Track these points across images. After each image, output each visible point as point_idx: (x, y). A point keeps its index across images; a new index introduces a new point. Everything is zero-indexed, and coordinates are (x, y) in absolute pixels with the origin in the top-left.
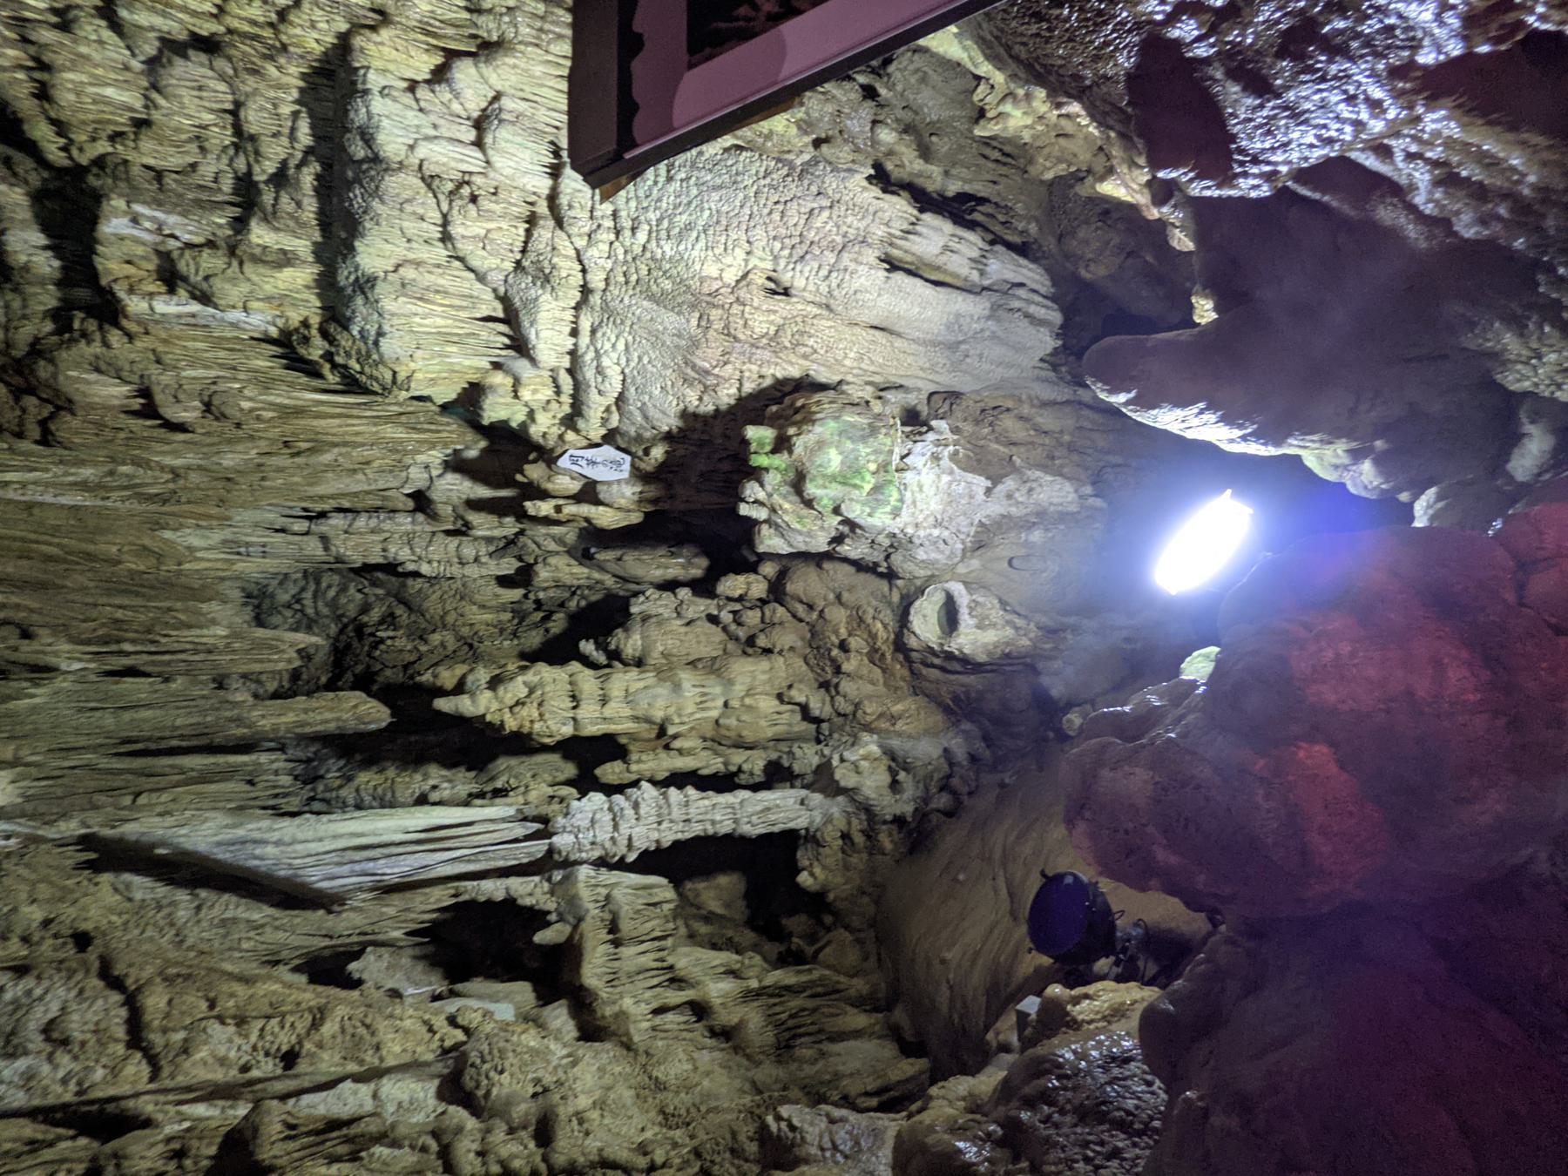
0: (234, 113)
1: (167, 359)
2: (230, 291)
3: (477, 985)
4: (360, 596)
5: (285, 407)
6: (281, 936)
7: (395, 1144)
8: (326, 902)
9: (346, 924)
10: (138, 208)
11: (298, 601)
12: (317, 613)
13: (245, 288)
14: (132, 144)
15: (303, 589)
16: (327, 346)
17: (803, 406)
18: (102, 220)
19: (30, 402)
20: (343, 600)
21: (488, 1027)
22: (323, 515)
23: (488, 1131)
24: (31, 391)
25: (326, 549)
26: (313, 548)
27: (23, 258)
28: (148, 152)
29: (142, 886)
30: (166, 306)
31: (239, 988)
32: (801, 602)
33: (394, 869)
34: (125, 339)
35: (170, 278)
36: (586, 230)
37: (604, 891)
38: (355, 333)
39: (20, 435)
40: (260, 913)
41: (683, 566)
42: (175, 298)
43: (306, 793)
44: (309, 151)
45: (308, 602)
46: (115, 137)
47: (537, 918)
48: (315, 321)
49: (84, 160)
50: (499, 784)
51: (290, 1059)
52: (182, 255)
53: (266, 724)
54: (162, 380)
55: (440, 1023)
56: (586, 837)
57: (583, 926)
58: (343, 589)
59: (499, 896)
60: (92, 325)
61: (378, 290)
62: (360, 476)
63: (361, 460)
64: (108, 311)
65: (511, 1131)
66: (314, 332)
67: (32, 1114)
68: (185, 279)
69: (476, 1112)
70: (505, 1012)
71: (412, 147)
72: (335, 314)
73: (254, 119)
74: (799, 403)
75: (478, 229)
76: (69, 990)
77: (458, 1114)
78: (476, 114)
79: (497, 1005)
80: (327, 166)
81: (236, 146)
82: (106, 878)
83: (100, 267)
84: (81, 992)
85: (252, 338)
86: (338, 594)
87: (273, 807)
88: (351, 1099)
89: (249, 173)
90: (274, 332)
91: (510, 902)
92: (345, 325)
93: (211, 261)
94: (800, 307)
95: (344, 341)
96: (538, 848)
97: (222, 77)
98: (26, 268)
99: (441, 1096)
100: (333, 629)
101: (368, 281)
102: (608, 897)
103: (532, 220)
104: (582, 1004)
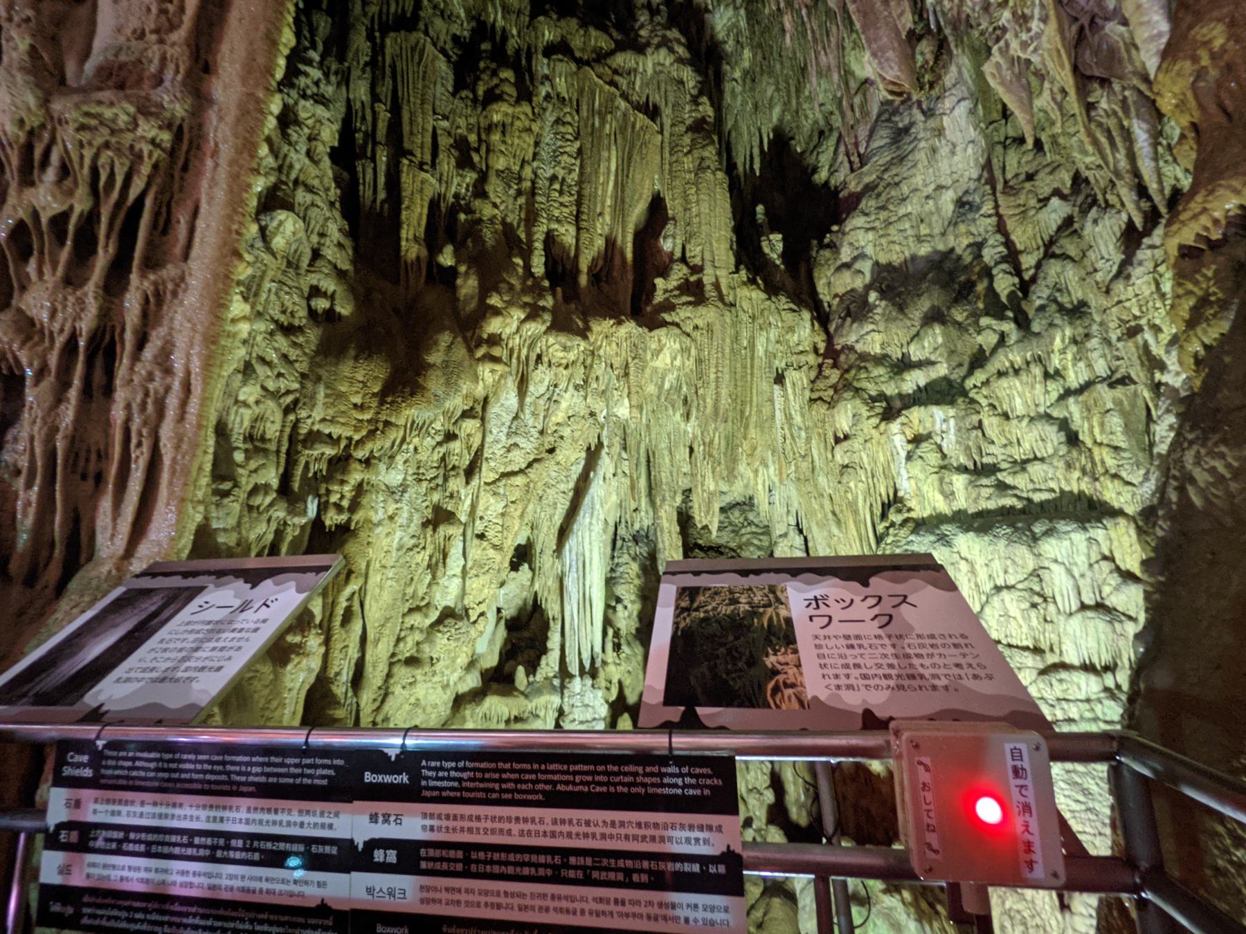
0: (1036, 458)
2: (916, 468)
3: (502, 632)
6: (545, 529)
7: (430, 585)
8: (559, 550)
9: (546, 560)
10: (952, 422)
13: (921, 476)
17: (937, 913)
19: (831, 392)
21: (473, 633)
22: (801, 531)
23: (421, 631)
24: (836, 391)
26: (779, 529)
28: (991, 424)
29: (577, 469)
31: (519, 513)
32: (765, 914)
33: (570, 583)
36: (1045, 695)
37: (542, 714)
40: (558, 519)
41: (797, 800)
43: (628, 537)
44: (1029, 500)
46: (993, 407)
47: (532, 668)
48: (913, 515)
49: (972, 394)
50: (624, 647)
51: (481, 536)
53: (662, 513)
54: (856, 444)
55: (483, 608)
56: (576, 701)
57: (522, 698)
58: (759, 548)
59: (549, 645)
64: (889, 415)
65: (418, 643)
67: (482, 445)
69: (432, 626)
70: (482, 647)
71: (1056, 561)
73: (1035, 469)
74: (939, 908)
75: (1014, 610)
77: (434, 615)
78: (1107, 603)
79: (486, 642)
80: (1023, 511)
81: (1015, 462)
82: (583, 455)
88: (455, 563)
89: (1000, 470)
90: (900, 494)
91: (544, 650)
92: (915, 531)
93: (934, 459)
94: (1053, 923)
95: (903, 532)
96: (574, 668)
97: (1056, 451)
99: (447, 608)
100: (733, 545)
102: (537, 716)
103: (1037, 651)
104: (476, 696)
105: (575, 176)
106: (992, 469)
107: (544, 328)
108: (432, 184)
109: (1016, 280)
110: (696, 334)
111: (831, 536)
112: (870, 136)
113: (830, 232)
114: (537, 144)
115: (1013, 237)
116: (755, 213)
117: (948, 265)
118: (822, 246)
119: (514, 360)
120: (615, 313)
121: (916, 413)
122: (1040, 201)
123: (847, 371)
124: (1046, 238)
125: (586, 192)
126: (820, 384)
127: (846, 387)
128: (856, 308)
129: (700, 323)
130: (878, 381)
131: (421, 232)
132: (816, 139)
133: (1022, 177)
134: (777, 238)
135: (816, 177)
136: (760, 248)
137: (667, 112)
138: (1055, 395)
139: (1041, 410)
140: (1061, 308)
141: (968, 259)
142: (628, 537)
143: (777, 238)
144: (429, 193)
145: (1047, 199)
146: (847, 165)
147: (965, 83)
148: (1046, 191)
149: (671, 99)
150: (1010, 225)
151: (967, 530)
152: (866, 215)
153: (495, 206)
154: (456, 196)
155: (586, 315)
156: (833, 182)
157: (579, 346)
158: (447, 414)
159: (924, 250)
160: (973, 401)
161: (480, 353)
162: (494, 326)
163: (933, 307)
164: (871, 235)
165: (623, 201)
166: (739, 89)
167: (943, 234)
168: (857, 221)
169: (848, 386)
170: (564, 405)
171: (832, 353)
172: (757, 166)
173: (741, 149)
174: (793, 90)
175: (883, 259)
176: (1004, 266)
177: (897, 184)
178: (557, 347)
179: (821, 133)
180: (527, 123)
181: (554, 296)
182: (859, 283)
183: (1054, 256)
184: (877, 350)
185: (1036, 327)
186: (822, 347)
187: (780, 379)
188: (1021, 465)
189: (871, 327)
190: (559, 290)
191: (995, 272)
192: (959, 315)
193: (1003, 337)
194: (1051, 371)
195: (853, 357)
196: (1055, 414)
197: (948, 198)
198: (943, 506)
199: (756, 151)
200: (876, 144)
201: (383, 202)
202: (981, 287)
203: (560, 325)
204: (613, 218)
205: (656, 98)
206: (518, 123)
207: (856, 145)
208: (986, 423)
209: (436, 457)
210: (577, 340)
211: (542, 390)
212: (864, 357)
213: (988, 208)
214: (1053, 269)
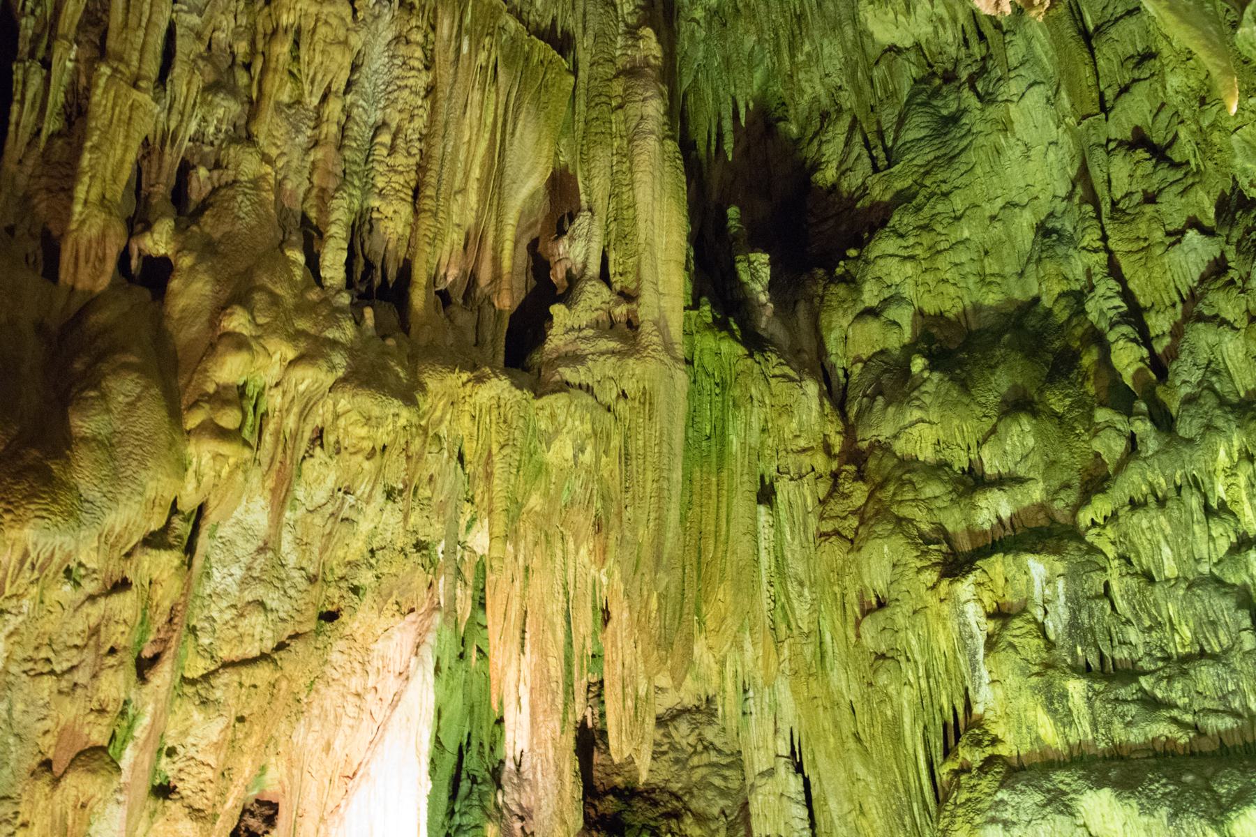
1: (920, 619)
2: (1007, 664)
4: (716, 811)
5: (901, 727)
10: (1061, 583)
11: (706, 748)
12: (693, 768)
14: (1124, 572)
15: (719, 752)
16: (978, 764)
18: (1037, 557)
19: (854, 522)
20: (709, 794)
22: (799, 768)
25: (762, 774)
26: (759, 761)
27: (983, 504)
30: (974, 614)
34: (930, 585)
35: (1001, 614)
38: (1000, 795)
39: (822, 518)
42: (984, 620)
43: (482, 774)
45: (705, 758)
48: (1002, 750)
52: (1029, 622)
58: (724, 793)
60: (936, 557)
61: (1059, 817)
62: (847, 806)
63: (866, 807)
64: (956, 565)
66: (989, 751)
68: (1004, 627)
72: (1014, 772)
76: (287, 612)
80: (1192, 753)
81: (1167, 658)
83: (993, 558)
84: (283, 620)
85: (967, 689)
86: (717, 788)
87: (469, 744)
90: (978, 710)
95: (985, 784)
98: (974, 507)
100: (675, 787)
101: (1067, 806)
105: (419, 123)
106: (1129, 673)
107: (330, 380)
108: (150, 113)
109: (1145, 352)
110: (621, 407)
111: (854, 780)
112: (901, 122)
113: (846, 258)
114: (355, 67)
115: (1131, 286)
116: (724, 217)
117: (1032, 322)
118: (832, 279)
119: (268, 438)
120: (469, 361)
121: (998, 565)
122: (1169, 234)
123: (881, 486)
124: (1185, 291)
125: (437, 152)
126: (837, 507)
127: (876, 515)
128: (891, 380)
129: (630, 386)
130: (929, 505)
131: (118, 191)
132: (816, 123)
133: (1138, 198)
134: (761, 259)
135: (818, 176)
136: (735, 273)
137: (585, 47)
138: (1223, 545)
139: (1205, 569)
140: (1222, 402)
141: (1062, 315)
142: (482, 774)
143: (761, 259)
144: (144, 128)
145: (1182, 232)
146: (867, 161)
147: (1038, 62)
148: (1178, 222)
149: (593, 23)
150: (1126, 268)
151: (1099, 784)
152: (901, 236)
153: (266, 159)
154: (198, 138)
155: (414, 360)
156: (845, 185)
157: (396, 415)
158: (107, 541)
159: (992, 298)
160: (1093, 549)
161: (194, 420)
162: (230, 369)
163: (1015, 387)
164: (909, 268)
165: (501, 172)
166: (701, 34)
167: (1021, 275)
168: (886, 245)
169: (883, 513)
170: (365, 526)
171: (855, 458)
172: (728, 146)
173: (701, 119)
174: (784, 43)
175: (930, 307)
176: (1126, 329)
177: (946, 195)
178: (362, 418)
179: (825, 116)
180: (341, 33)
181: (358, 322)
182: (895, 341)
183: (1201, 318)
184: (927, 454)
185: (1186, 428)
186: (837, 441)
187: (766, 495)
188: (1182, 665)
189: (917, 414)
190: (369, 313)
191: (1111, 337)
192: (1057, 402)
193: (1133, 441)
194: (1214, 505)
195: (890, 463)
196: (1231, 578)
197: (1025, 222)
198: (1050, 734)
199: (727, 125)
200: (910, 135)
201: (51, 137)
202: (1089, 359)
203: (365, 375)
204: (482, 199)
205: (572, 23)
206: (322, 30)
207: (881, 134)
208: (1115, 587)
209: (80, 624)
210: (395, 405)
211: (321, 496)
212: (908, 464)
213: (1091, 237)
214: (1203, 337)
